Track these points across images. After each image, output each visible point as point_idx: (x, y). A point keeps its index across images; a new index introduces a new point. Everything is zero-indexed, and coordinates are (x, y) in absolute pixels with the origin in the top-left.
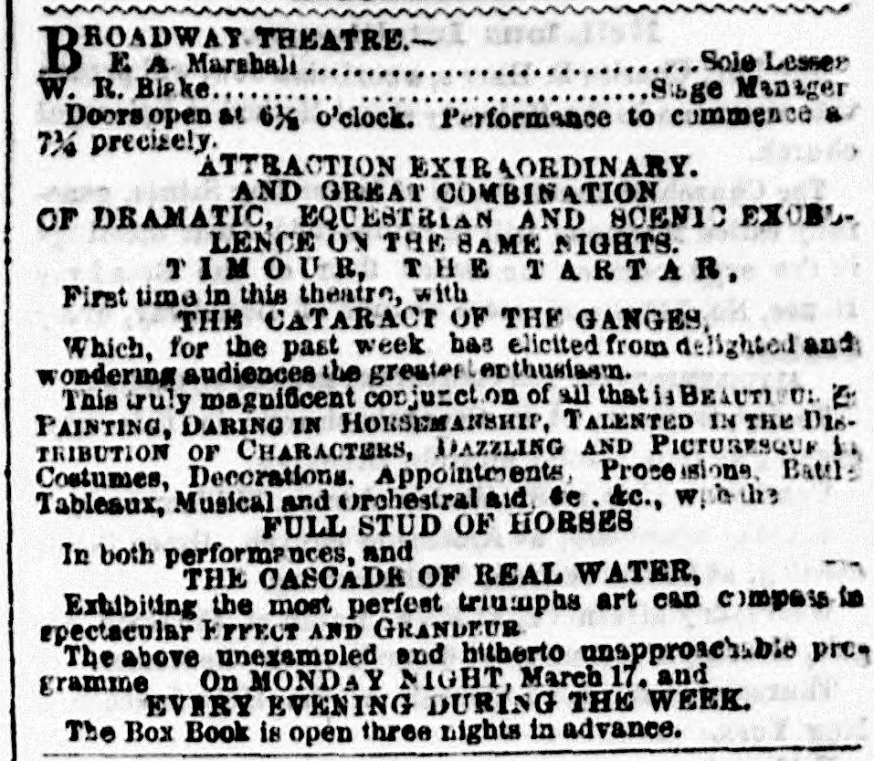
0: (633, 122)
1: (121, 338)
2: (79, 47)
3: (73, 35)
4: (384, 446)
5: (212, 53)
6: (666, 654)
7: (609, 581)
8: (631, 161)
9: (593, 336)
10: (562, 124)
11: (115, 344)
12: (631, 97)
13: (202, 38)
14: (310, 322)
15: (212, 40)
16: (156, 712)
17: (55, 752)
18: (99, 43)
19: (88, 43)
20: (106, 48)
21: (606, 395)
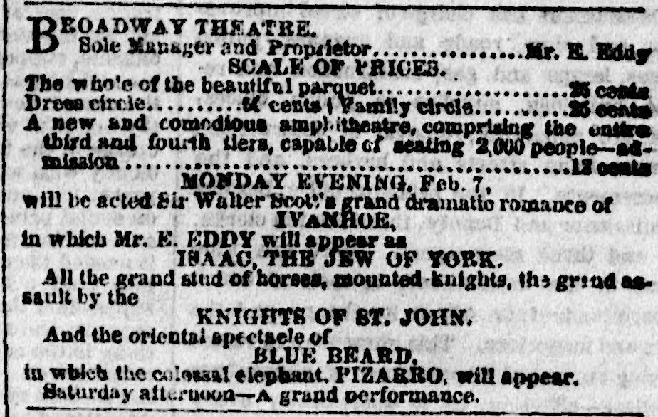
1: (91, 365)
2: (57, 32)
3: (53, 24)
4: (199, 392)
6: (404, 262)
9: (88, 135)
11: (87, 369)
13: (152, 26)
15: (161, 28)
16: (309, 360)
17: (215, 409)
19: (64, 31)
21: (99, 336)
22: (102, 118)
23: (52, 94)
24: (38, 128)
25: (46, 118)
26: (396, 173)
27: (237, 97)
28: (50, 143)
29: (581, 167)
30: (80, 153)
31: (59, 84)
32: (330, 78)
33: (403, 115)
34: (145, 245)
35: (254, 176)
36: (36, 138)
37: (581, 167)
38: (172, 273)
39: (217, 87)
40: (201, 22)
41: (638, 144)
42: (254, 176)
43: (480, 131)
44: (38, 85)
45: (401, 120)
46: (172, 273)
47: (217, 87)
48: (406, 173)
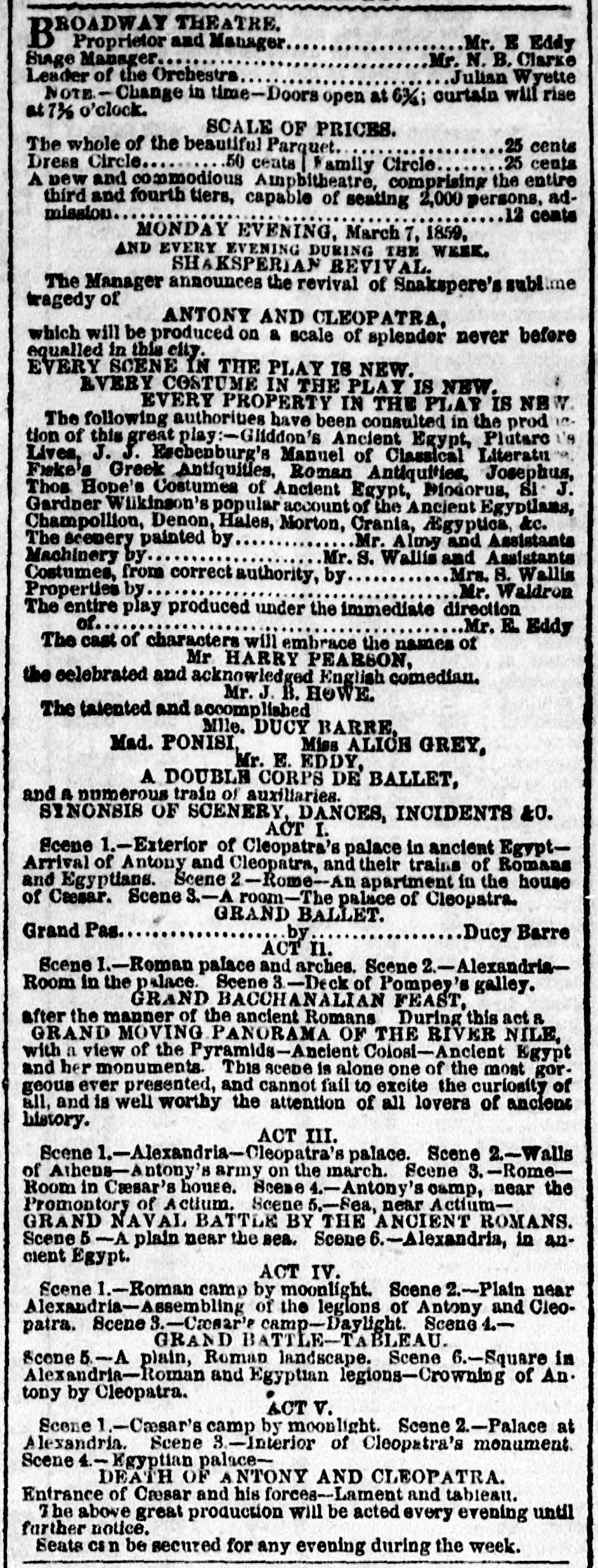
0: (524, 341)
3: (48, 21)
5: (227, 34)
7: (229, 1037)
8: (339, 725)
10: (468, 99)
12: (437, 82)
13: (138, 23)
14: (235, 25)
15: (145, 25)
18: (66, 28)
20: (71, 31)
22: (404, 870)
23: (52, 155)
24: (40, 183)
25: (44, 174)
26: (325, 222)
27: (220, 157)
28: (50, 197)
29: (513, 216)
30: (75, 205)
31: (56, 144)
32: (293, 138)
33: (367, 172)
34: (109, 901)
35: (201, 224)
36: (38, 192)
37: (513, 216)
38: (184, 669)
39: (198, 144)
40: (180, 18)
41: (567, 193)
42: (201, 224)
43: (440, 186)
44: (39, 145)
45: (363, 177)
46: (184, 669)
47: (198, 144)
48: (332, 223)
